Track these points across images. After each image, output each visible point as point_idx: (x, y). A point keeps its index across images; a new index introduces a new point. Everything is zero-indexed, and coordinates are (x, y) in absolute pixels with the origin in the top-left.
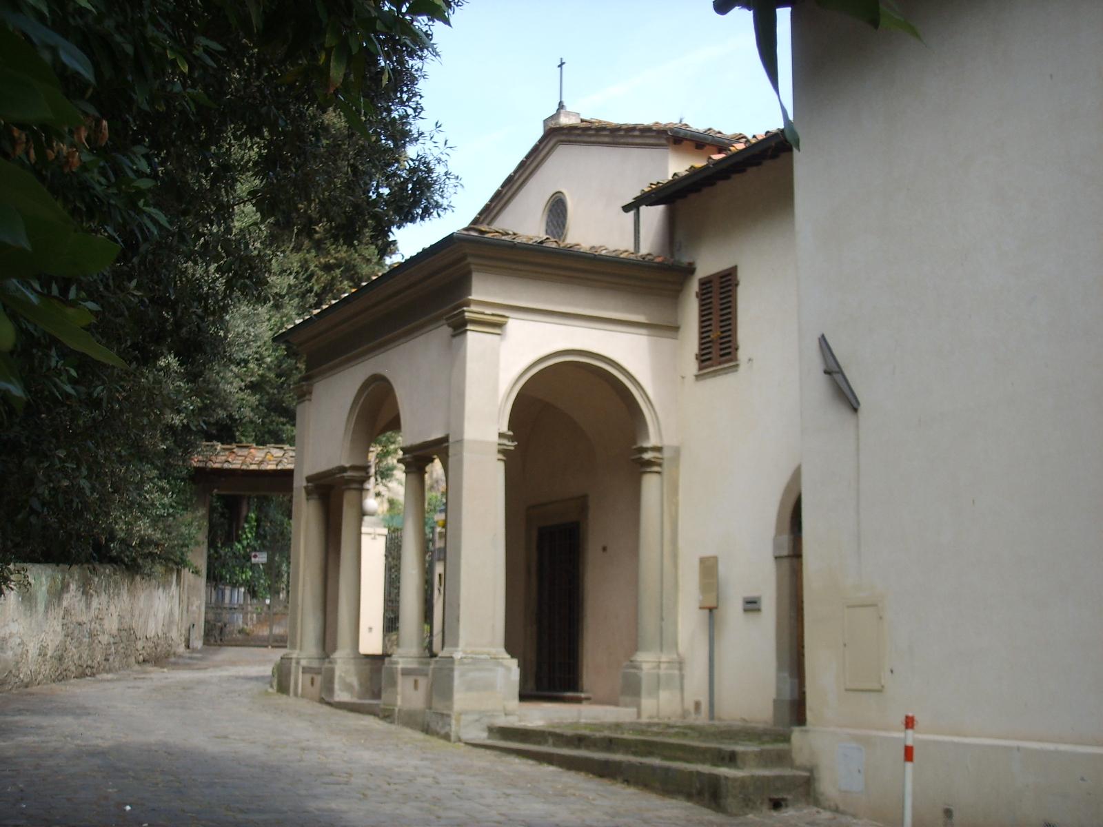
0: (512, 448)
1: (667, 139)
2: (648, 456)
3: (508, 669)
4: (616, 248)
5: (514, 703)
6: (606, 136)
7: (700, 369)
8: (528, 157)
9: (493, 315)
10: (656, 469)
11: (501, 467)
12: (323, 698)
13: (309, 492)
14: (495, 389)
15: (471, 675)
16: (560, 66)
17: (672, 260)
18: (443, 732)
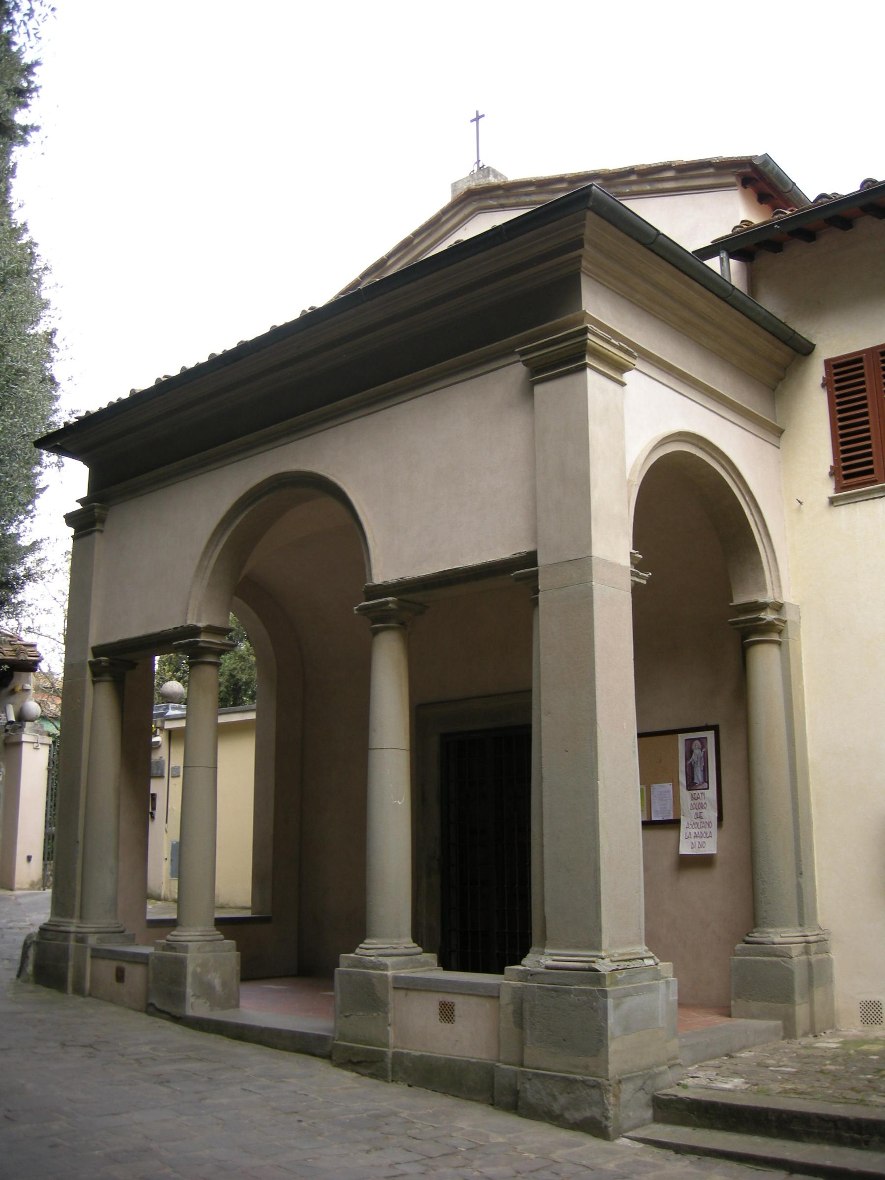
0: (644, 582)
2: (769, 616)
7: (839, 488)
8: (417, 234)
10: (775, 637)
12: (152, 1005)
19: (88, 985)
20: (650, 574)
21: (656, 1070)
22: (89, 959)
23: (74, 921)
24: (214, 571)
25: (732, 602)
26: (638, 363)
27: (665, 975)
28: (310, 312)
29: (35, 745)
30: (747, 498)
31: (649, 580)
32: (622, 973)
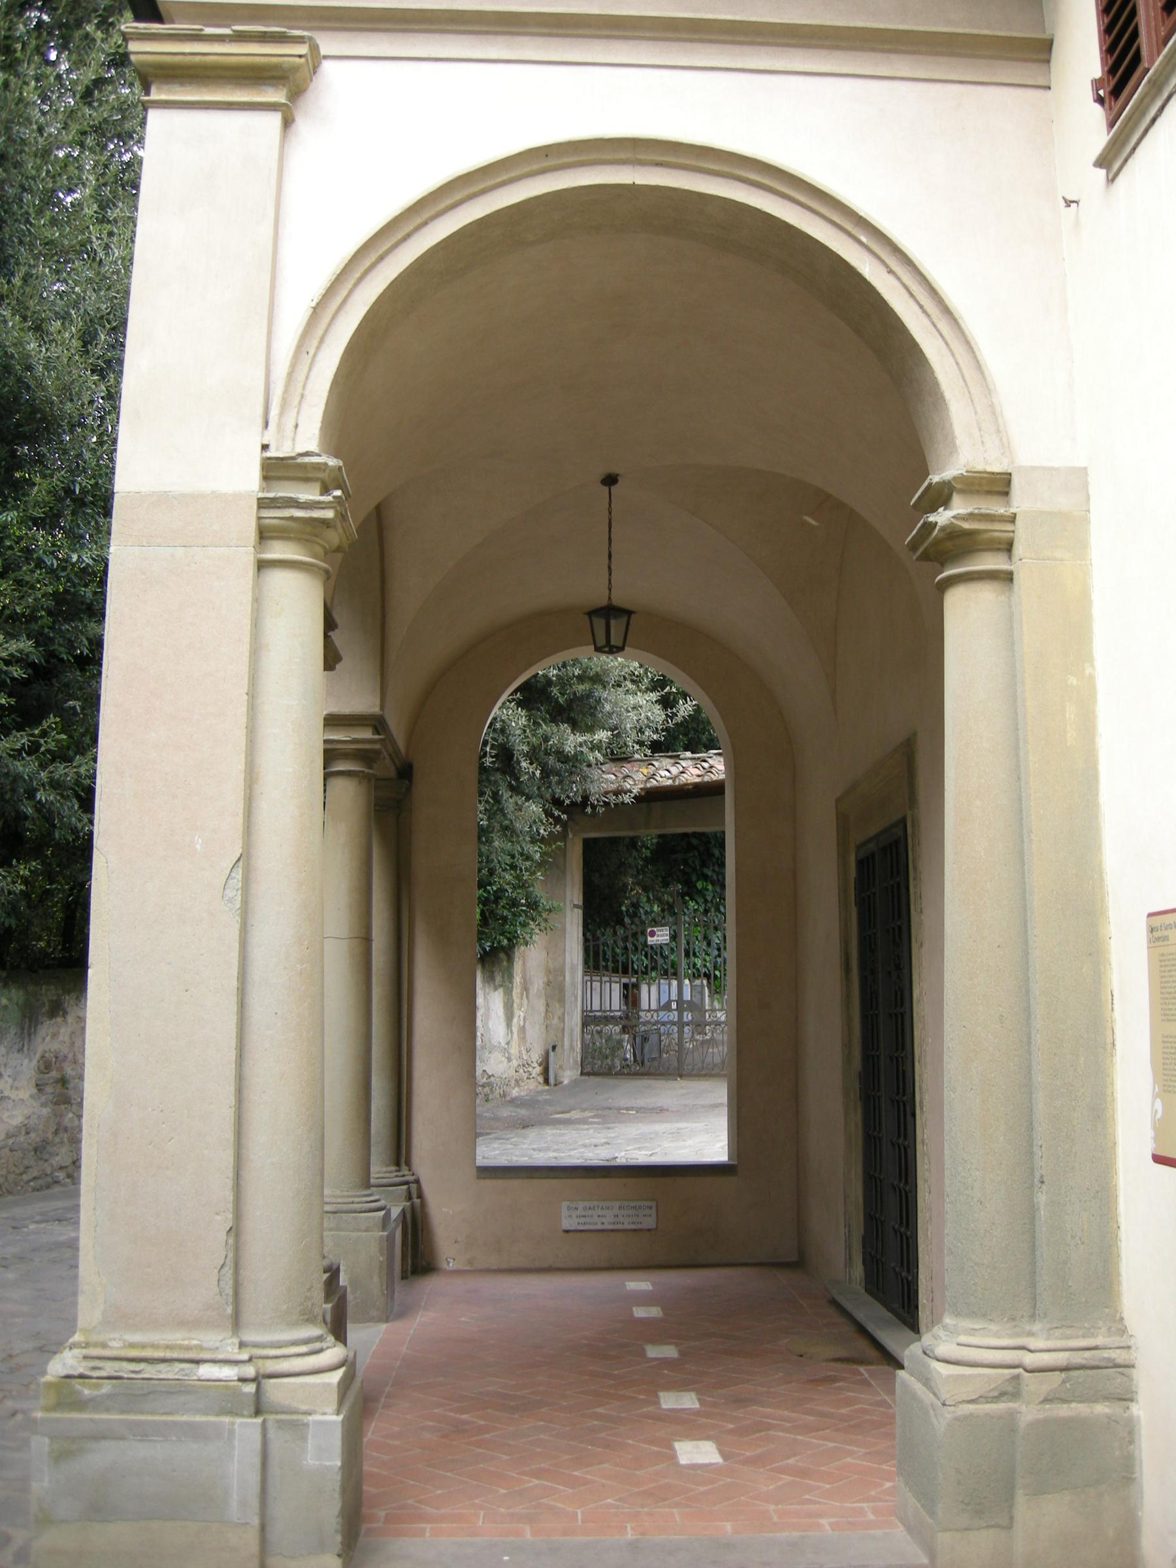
15: (102, 1456)
26: (328, 44)
27: (304, 1407)
28: (343, 1419)
30: (863, 239)
32: (97, 1386)
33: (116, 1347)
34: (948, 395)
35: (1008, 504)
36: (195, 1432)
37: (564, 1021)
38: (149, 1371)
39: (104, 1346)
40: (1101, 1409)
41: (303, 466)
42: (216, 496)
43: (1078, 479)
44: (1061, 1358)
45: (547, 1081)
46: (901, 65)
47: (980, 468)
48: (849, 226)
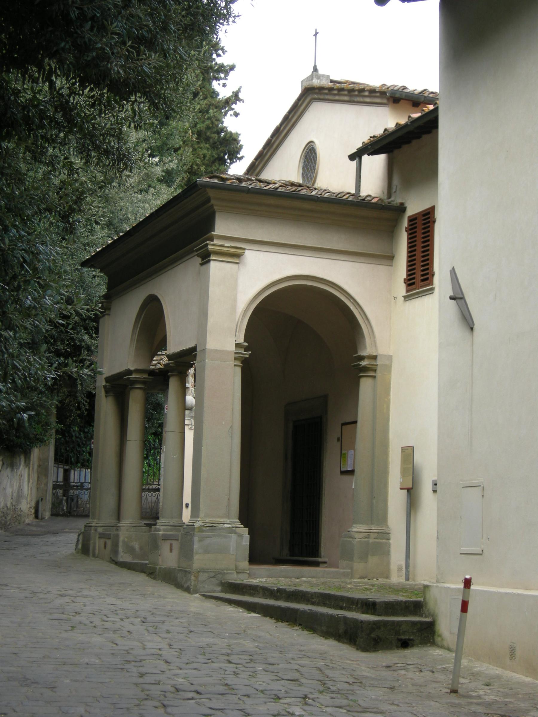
0: (248, 356)
1: (388, 99)
2: (363, 363)
3: (240, 536)
4: (341, 191)
5: (245, 564)
6: (345, 95)
7: (407, 291)
8: (290, 112)
9: (232, 247)
10: (372, 374)
11: (238, 371)
13: (107, 391)
14: (234, 308)
15: (208, 541)
16: (315, 35)
17: (386, 201)
18: (186, 586)
19: (97, 552)
20: (250, 352)
21: (225, 571)
22: (97, 539)
23: (95, 521)
24: (137, 341)
25: (357, 353)
29: (190, 426)
31: (250, 355)
33: (207, 521)
34: (366, 337)
35: (376, 362)
36: (225, 537)
37: (47, 486)
38: (218, 525)
39: (205, 521)
40: (384, 541)
41: (242, 345)
42: (227, 351)
43: (390, 358)
44: (377, 531)
45: (37, 517)
46: (362, 259)
47: (371, 354)
48: (349, 298)
